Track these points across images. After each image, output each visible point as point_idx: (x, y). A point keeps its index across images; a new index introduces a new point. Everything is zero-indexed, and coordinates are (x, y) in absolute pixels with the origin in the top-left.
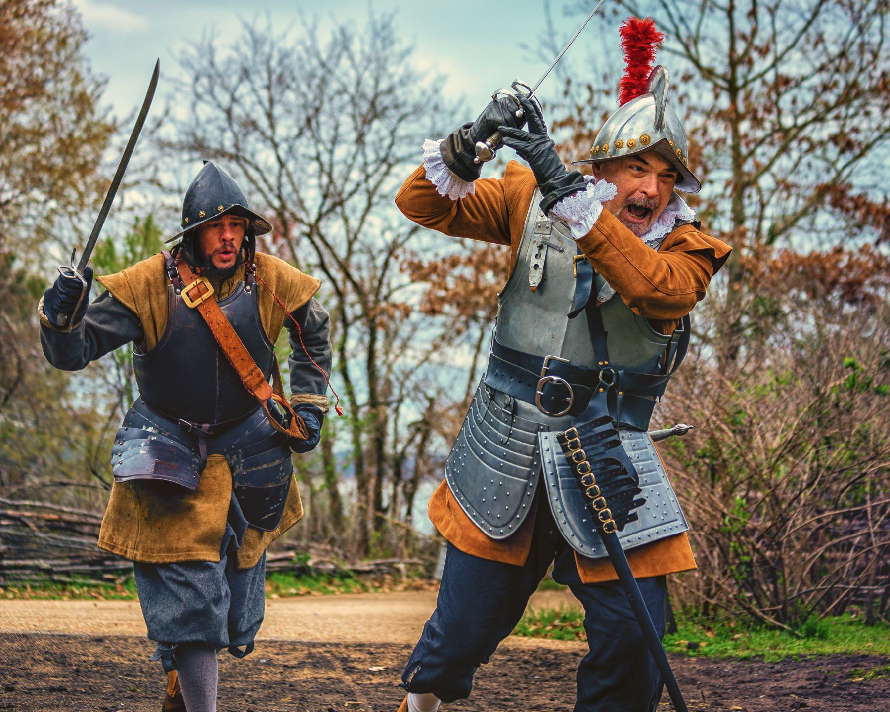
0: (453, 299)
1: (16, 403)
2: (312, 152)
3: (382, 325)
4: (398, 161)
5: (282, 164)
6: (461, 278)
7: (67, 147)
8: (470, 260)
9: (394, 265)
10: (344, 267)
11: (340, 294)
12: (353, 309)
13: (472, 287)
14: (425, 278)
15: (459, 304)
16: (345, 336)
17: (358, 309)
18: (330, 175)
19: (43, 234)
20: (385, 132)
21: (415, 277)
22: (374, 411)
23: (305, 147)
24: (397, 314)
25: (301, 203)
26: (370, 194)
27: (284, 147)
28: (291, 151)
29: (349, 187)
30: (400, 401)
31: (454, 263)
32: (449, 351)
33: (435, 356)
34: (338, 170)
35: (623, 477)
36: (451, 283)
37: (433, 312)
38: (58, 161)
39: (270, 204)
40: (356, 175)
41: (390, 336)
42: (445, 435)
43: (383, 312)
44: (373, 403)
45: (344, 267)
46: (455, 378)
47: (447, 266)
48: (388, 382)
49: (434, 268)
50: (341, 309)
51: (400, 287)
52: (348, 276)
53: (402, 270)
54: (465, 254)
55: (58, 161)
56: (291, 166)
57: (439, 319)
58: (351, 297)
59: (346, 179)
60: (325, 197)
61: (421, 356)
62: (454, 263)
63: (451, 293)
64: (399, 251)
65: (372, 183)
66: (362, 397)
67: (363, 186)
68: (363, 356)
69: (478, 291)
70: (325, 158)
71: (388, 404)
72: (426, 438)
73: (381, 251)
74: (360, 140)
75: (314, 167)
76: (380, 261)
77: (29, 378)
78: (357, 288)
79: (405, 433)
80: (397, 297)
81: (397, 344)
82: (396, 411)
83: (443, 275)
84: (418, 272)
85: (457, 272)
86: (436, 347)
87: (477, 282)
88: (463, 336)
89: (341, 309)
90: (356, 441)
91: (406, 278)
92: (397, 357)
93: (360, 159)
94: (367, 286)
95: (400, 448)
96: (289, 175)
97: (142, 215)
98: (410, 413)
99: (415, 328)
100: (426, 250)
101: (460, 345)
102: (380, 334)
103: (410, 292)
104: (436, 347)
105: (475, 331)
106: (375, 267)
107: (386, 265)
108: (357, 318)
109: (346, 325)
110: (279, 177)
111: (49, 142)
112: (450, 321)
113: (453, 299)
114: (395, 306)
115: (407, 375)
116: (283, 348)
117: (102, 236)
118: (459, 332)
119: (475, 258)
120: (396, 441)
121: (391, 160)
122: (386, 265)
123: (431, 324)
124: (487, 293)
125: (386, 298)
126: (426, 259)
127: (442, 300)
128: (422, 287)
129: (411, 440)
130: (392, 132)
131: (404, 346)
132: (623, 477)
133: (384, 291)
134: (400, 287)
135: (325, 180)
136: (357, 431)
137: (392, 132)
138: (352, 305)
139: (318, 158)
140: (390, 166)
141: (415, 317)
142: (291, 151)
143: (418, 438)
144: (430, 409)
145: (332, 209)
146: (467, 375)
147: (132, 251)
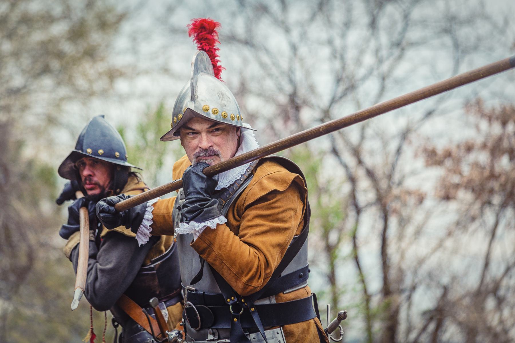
0: (469, 185)
1: (23, 290)
2: (324, 36)
3: (395, 211)
4: (412, 44)
5: (294, 48)
6: (476, 165)
7: (77, 33)
8: (484, 146)
9: (408, 151)
10: (356, 152)
11: (352, 180)
12: (366, 194)
13: (487, 173)
14: (440, 163)
15: (473, 190)
16: (357, 222)
17: (371, 196)
18: (342, 58)
19: (51, 121)
20: (398, 16)
21: (430, 162)
22: (386, 301)
23: (317, 31)
24: (412, 201)
25: (312, 88)
26: (383, 78)
27: (295, 34)
28: (303, 36)
29: (361, 72)
30: (414, 288)
31: (469, 149)
32: (465, 238)
33: (449, 243)
34: (351, 55)
35: (128, 232)
36: (466, 170)
37: (447, 198)
38: (67, 47)
39: (281, 89)
40: (369, 60)
41: (403, 222)
42: (460, 324)
43: (397, 198)
44: (387, 291)
45: (356, 152)
46: (469, 266)
47: (462, 153)
48: (401, 271)
49: (448, 154)
50: (353, 195)
51: (414, 173)
52: (360, 162)
53: (416, 156)
54: (479, 140)
55: (67, 47)
56: (303, 50)
57: (453, 206)
58: (364, 183)
59: (358, 62)
60: (339, 80)
61: (434, 243)
62: (469, 149)
63: (465, 180)
64: (413, 137)
65: (385, 67)
66: (375, 285)
67: (375, 73)
68: (375, 245)
69: (493, 176)
70: (338, 42)
71: (401, 291)
72: (439, 326)
73: (394, 137)
74: (373, 24)
75: (325, 52)
76: (393, 146)
77: (39, 265)
78: (370, 174)
79: (418, 322)
80: (411, 183)
81: (410, 230)
82: (409, 298)
83: (458, 161)
84: (433, 158)
85: (472, 157)
86: (450, 234)
87: (492, 167)
88: (477, 223)
89: (353, 195)
90: (369, 329)
91: (420, 163)
92: (411, 244)
93: (373, 44)
94: (379, 173)
95: (413, 336)
96: (301, 60)
97: (154, 104)
98: (424, 300)
99: (428, 215)
100: (440, 135)
101: (475, 231)
102: (393, 222)
103: (424, 179)
104: (450, 234)
105: (490, 217)
106: (387, 155)
107: (399, 151)
108: (369, 205)
109: (358, 211)
110: (291, 60)
111: (59, 29)
112: (464, 208)
113: (469, 185)
114: (409, 193)
115: (421, 262)
116: (178, 171)
117: (201, 174)
118: (473, 219)
119: (490, 144)
120: (409, 330)
121: (404, 43)
122: (399, 151)
123: (444, 212)
124: (503, 179)
125: (400, 184)
126: (440, 146)
127: (457, 186)
128: (435, 174)
129: (424, 329)
130: (406, 17)
131: (418, 233)
132: (128, 232)
133: (396, 177)
134: (414, 173)
135: (337, 65)
136: (369, 318)
137: (406, 17)
138: (365, 191)
139: (330, 42)
140: (403, 49)
141: (428, 203)
142: (303, 36)
143: (432, 327)
144: (445, 294)
145: (344, 94)
146: (481, 263)
147: (144, 137)
